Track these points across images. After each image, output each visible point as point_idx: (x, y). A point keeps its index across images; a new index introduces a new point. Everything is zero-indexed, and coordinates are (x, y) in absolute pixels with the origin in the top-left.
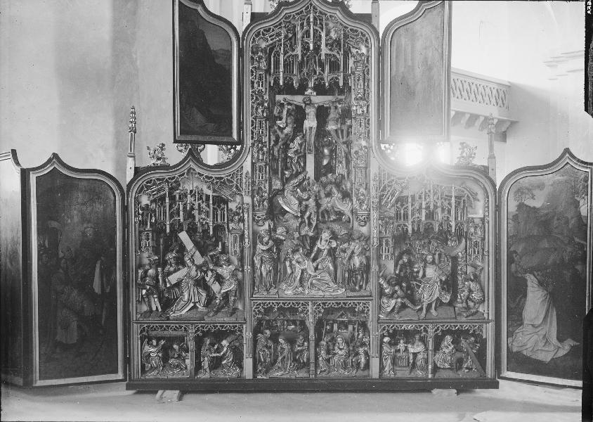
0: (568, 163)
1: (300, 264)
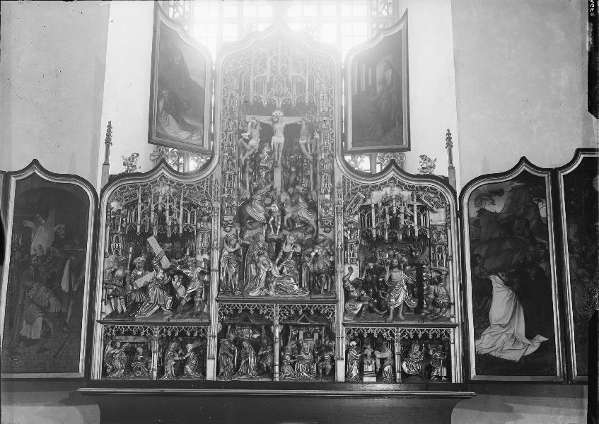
1: (265, 267)
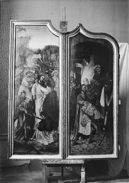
0: (12, 22)
